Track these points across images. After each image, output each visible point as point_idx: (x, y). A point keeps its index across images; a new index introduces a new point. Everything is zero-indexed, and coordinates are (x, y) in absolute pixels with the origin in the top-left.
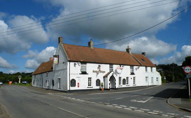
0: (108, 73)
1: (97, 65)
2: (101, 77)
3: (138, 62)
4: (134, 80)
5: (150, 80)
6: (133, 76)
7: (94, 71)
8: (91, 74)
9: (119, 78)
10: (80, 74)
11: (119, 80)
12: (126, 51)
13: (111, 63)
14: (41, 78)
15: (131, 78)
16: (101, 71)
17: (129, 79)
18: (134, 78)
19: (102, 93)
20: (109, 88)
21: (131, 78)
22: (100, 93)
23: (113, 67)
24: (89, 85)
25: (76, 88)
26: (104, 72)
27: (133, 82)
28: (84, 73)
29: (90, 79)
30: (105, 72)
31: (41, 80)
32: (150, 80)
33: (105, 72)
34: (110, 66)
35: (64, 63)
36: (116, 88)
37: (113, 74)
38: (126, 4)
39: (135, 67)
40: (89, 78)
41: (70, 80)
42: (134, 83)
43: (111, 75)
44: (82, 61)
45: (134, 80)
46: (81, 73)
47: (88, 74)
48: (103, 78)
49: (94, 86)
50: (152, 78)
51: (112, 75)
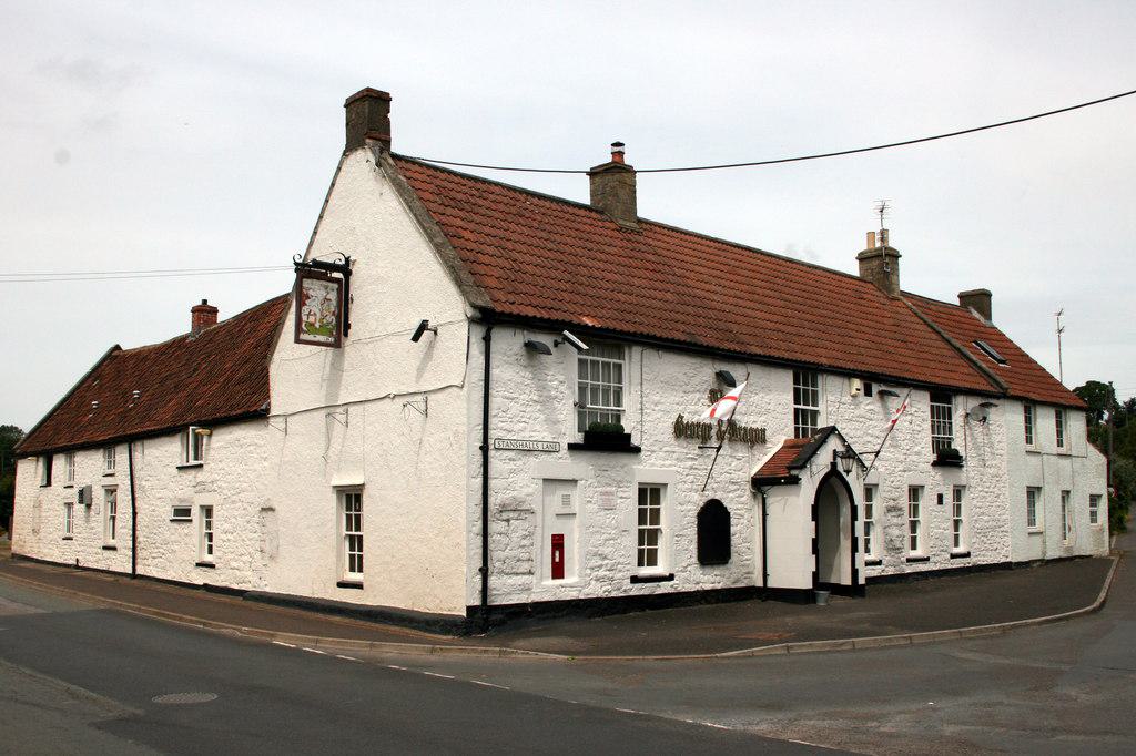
2: (733, 472)
3: (970, 360)
7: (683, 430)
8: (660, 459)
9: (642, 500)
10: (572, 447)
11: (642, 513)
12: (579, 191)
13: (873, 369)
15: (940, 499)
17: (927, 502)
19: (1106, 585)
21: (940, 499)
22: (1111, 573)
23: (815, 394)
26: (756, 438)
27: (631, 543)
28: (606, 439)
29: (650, 494)
31: (123, 497)
33: (764, 441)
34: (796, 381)
36: (862, 581)
43: (823, 461)
44: (589, 322)
46: (578, 438)
48: (748, 487)
49: (678, 564)
50: (1066, 494)
51: (834, 465)
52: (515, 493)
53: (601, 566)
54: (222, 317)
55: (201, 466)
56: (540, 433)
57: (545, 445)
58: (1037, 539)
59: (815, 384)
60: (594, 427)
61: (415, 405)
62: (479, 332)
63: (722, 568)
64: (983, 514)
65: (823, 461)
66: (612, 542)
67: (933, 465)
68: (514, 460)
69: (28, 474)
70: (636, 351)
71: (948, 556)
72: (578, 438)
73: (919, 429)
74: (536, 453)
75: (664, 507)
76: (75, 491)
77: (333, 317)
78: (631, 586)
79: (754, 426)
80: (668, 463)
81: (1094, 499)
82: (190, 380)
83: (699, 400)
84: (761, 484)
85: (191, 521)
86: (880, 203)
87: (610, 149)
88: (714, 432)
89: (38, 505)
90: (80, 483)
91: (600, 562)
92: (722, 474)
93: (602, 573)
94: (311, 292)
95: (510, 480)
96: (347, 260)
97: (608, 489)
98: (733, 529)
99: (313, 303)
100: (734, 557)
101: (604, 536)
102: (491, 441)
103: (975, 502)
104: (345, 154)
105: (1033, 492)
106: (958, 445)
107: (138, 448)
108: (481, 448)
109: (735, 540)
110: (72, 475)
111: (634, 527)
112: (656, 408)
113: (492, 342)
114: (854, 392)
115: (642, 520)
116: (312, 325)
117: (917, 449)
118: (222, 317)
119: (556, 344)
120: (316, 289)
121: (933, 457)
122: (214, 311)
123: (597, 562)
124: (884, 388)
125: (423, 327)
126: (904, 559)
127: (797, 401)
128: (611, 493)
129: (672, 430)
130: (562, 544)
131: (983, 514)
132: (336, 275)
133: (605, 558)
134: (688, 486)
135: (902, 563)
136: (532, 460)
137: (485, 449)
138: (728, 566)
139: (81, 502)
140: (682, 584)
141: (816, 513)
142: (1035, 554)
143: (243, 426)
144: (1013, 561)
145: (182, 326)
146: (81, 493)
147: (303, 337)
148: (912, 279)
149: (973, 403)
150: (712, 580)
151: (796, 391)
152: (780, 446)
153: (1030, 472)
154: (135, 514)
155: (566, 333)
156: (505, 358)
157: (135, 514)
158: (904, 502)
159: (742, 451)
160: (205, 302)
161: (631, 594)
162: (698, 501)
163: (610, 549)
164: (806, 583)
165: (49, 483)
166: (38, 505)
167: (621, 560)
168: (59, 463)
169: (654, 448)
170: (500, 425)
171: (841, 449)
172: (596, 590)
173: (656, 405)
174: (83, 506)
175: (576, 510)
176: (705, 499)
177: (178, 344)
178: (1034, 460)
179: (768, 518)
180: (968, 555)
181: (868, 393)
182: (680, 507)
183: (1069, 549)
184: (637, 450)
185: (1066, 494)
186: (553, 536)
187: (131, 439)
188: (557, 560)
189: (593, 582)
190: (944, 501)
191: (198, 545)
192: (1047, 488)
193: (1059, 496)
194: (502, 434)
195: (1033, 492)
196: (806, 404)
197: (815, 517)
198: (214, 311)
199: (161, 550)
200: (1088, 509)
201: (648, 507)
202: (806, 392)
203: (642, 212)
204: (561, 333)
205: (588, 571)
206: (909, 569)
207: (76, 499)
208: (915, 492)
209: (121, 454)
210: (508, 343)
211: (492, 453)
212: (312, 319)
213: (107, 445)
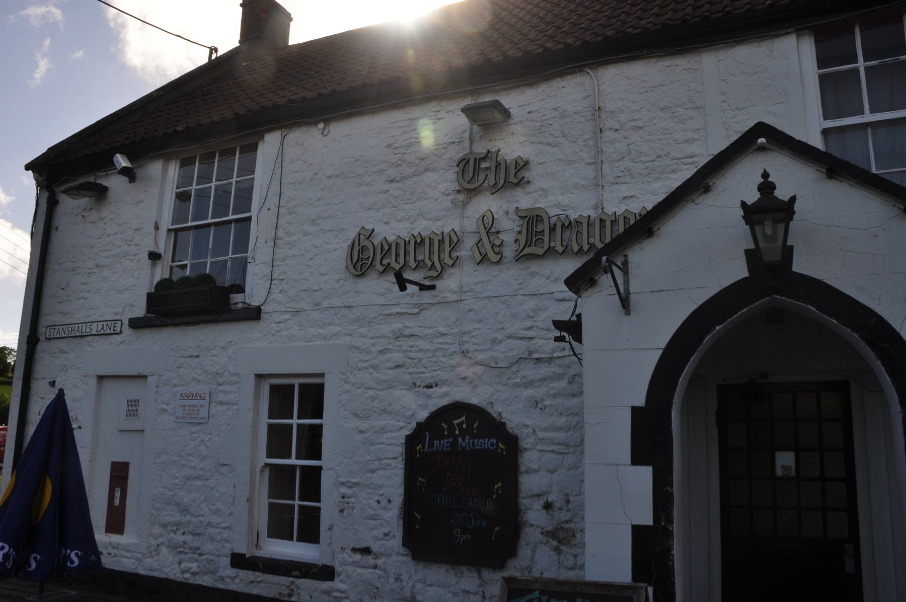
10: (136, 324)
53: (178, 524)
66: (199, 483)
74: (89, 339)
78: (232, 572)
91: (178, 517)
130: (126, 478)
143: (569, 77)
148: (749, 202)
161: (233, 587)
167: (215, 519)
169: (300, 305)
188: (117, 502)
189: (164, 550)
191: (75, 335)
201: (861, 64)
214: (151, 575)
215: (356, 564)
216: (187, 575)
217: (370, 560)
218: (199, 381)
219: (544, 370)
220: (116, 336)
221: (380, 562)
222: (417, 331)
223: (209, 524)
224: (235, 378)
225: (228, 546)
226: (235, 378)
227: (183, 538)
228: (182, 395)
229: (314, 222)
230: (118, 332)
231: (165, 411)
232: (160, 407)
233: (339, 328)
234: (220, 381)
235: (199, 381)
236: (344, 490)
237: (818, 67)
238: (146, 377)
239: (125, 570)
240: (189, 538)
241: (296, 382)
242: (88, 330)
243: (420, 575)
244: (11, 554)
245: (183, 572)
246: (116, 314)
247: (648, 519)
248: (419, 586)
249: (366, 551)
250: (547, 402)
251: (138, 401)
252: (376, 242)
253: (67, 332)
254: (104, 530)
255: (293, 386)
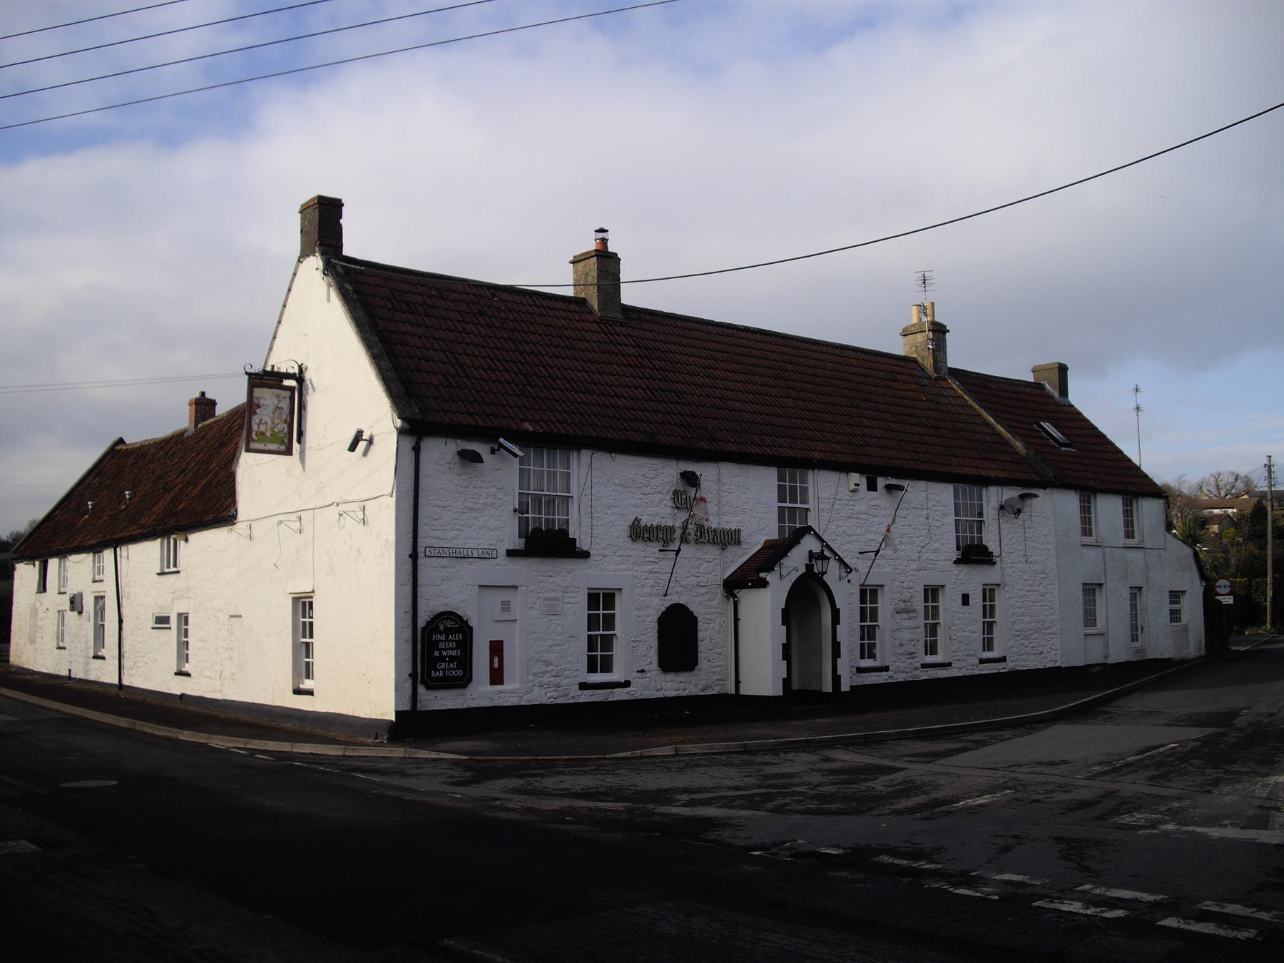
0: (769, 546)
1: (667, 473)
4: (989, 611)
5: (1112, 610)
6: (975, 579)
7: (639, 532)
10: (511, 553)
14: (109, 589)
15: (966, 600)
16: (700, 527)
17: (948, 603)
18: (989, 593)
20: (828, 687)
21: (966, 600)
24: (592, 668)
25: (481, 693)
26: (729, 539)
27: (978, 636)
30: (738, 542)
32: (1112, 610)
34: (781, 478)
35: (362, 445)
36: (845, 687)
37: (822, 557)
38: (114, 29)
39: (993, 497)
40: (593, 599)
41: (421, 624)
42: (988, 645)
43: (796, 561)
44: (528, 426)
45: (989, 611)
46: (519, 544)
47: (585, 555)
48: (720, 591)
50: (1136, 591)
51: (809, 567)
52: (447, 600)
53: (545, 673)
54: (221, 410)
55: (178, 572)
56: (479, 540)
57: (480, 551)
58: (1098, 641)
59: (804, 481)
60: (537, 530)
61: (352, 515)
62: (409, 443)
63: (687, 674)
64: (1023, 615)
65: (796, 561)
67: (955, 562)
68: (446, 567)
69: (25, 574)
70: (586, 454)
71: (977, 661)
72: (519, 544)
73: (938, 524)
74: (470, 560)
75: (618, 611)
76: (66, 598)
77: (285, 426)
78: (580, 692)
79: (727, 527)
80: (622, 567)
81: (1175, 596)
82: (177, 481)
83: (661, 502)
84: (734, 585)
85: (170, 628)
86: (920, 275)
87: (593, 235)
88: (678, 533)
89: (34, 612)
90: (72, 589)
91: (544, 669)
92: (687, 577)
93: (545, 680)
94: (262, 402)
95: (443, 587)
96: (300, 367)
97: (553, 595)
98: (700, 635)
99: (266, 412)
100: (703, 663)
101: (548, 643)
102: (420, 550)
103: (1012, 602)
104: (299, 261)
105: (1091, 590)
106: (990, 540)
107: (123, 551)
108: (410, 556)
109: (702, 647)
110: (62, 580)
111: (584, 634)
112: (610, 512)
113: (421, 452)
114: (852, 487)
115: (863, 619)
116: (263, 434)
117: (936, 545)
118: (221, 410)
119: (493, 451)
120: (267, 397)
121: (955, 555)
122: (213, 403)
123: (540, 668)
124: (893, 481)
125: (358, 437)
126: (918, 665)
127: (781, 498)
128: (557, 599)
129: (627, 533)
130: (502, 650)
131: (1023, 615)
132: (287, 383)
133: (550, 664)
134: (647, 590)
135: (916, 669)
136: (466, 566)
137: (414, 556)
138: (696, 672)
139: (72, 609)
140: (639, 690)
141: (786, 617)
142: (1095, 657)
144: (1063, 665)
145: (180, 420)
146: (72, 601)
147: (253, 445)
149: (1011, 493)
150: (675, 686)
151: (781, 490)
152: (759, 547)
153: (1087, 565)
154: (121, 621)
155: (502, 440)
156: (437, 467)
157: (121, 621)
158: (919, 603)
159: (711, 552)
160: (203, 394)
161: (581, 700)
162: (659, 605)
163: (555, 655)
164: (776, 690)
165: (45, 590)
166: (34, 612)
167: (568, 666)
168: (53, 563)
169: (607, 552)
170: (432, 533)
171: (816, 548)
172: (538, 697)
173: (609, 508)
174: (76, 613)
175: (517, 617)
176: (668, 604)
177: (177, 440)
178: (1092, 554)
179: (741, 623)
180: (1003, 659)
181: (872, 487)
182: (636, 613)
183: (1140, 651)
184: (585, 555)
185: (1136, 591)
186: (491, 642)
187: (116, 542)
188: (496, 665)
189: (536, 689)
190: (971, 601)
192: (1109, 585)
193: (1126, 593)
194: (435, 543)
195: (1091, 590)
196: (793, 500)
197: (786, 620)
198: (213, 403)
199: (145, 660)
200: (1167, 607)
202: (793, 489)
203: (622, 302)
204: (496, 440)
205: (531, 678)
206: (924, 675)
207: (67, 606)
208: (932, 593)
209: (108, 554)
210: (439, 452)
211: (421, 561)
212: (262, 428)
213: (96, 549)
214: (61, 704)
215: (639, 678)
216: (552, 700)
217: (644, 675)
218: (554, 591)
219: (704, 590)
220: (493, 560)
221: (648, 675)
222: (659, 570)
223: (566, 670)
224: (577, 590)
225: (577, 679)
226: (577, 590)
227: (548, 680)
228: (544, 598)
229: (609, 508)
230: (495, 557)
231: (533, 608)
232: (529, 605)
233: (626, 566)
234: (567, 590)
235: (554, 591)
236: (633, 644)
237: (808, 490)
238: (516, 587)
239: (513, 704)
240: (552, 679)
241: (601, 592)
242: (470, 553)
243: (663, 679)
244: (1241, 716)
245: (549, 698)
246: (491, 545)
247: (785, 642)
248: (663, 683)
249: (642, 671)
250: (705, 603)
251: (509, 602)
252: (643, 525)
253: (448, 553)
254: (489, 684)
255: (599, 594)
